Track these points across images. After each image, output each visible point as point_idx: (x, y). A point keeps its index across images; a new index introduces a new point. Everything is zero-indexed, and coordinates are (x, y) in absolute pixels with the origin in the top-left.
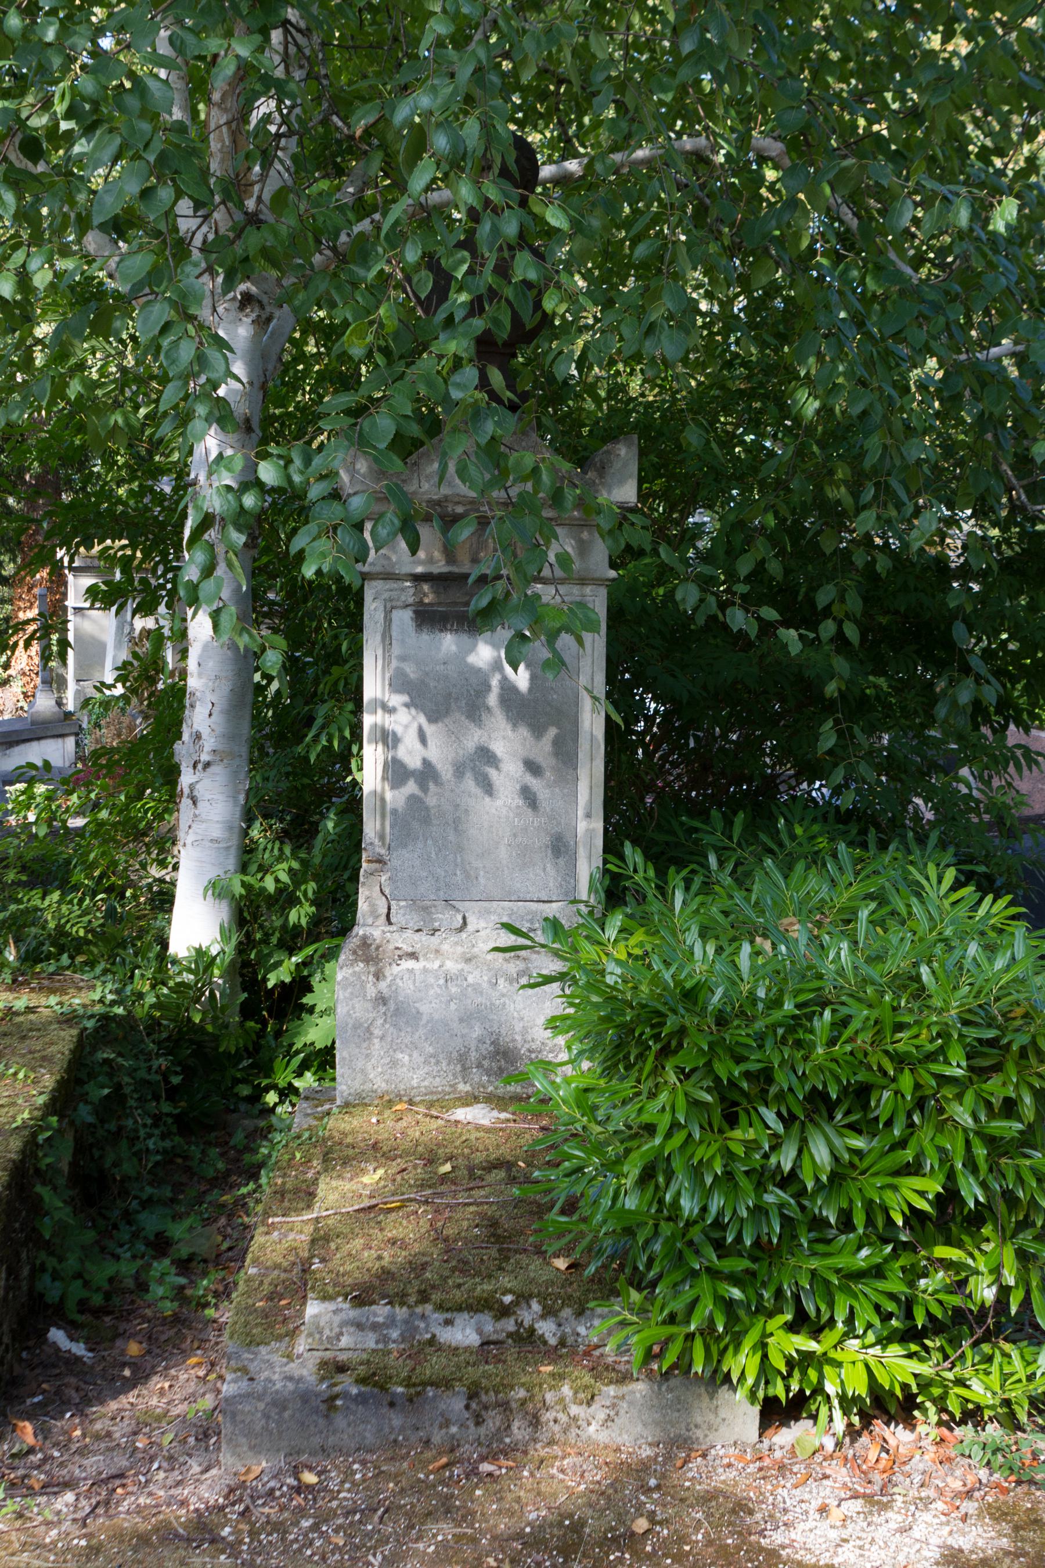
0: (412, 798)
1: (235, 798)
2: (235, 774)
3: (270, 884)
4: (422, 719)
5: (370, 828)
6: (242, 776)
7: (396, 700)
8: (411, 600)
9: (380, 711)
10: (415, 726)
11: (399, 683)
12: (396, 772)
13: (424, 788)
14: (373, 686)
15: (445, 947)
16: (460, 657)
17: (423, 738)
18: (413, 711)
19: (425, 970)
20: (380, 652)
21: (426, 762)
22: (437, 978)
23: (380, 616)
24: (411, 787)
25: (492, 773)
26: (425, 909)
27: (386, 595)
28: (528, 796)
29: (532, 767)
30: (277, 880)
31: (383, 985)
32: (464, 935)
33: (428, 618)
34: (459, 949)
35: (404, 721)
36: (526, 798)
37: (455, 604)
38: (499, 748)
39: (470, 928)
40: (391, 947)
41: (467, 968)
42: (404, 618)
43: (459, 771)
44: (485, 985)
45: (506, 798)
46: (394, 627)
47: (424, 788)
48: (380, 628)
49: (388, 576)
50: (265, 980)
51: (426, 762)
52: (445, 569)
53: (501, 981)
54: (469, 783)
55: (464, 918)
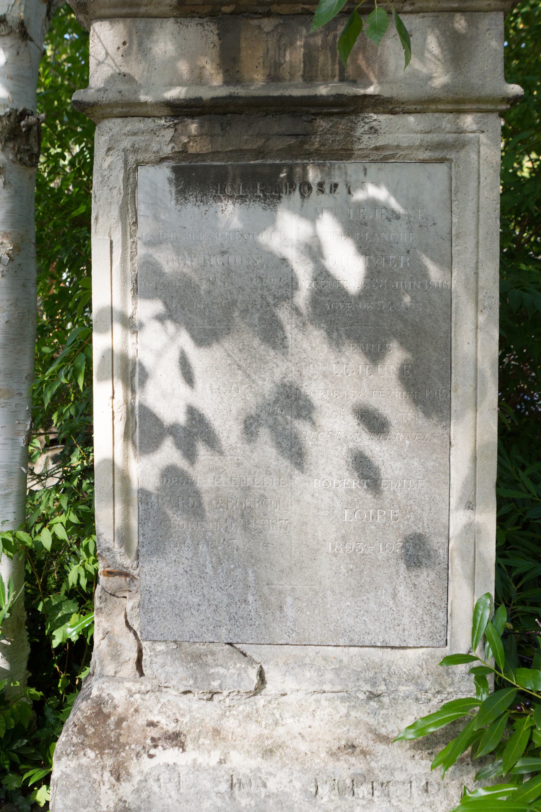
0: (170, 473)
1: (13, 440)
2: (14, 414)
3: (46, 539)
4: (185, 340)
5: (107, 517)
6: (22, 416)
7: (146, 309)
8: (167, 150)
9: (117, 328)
10: (173, 356)
11: (146, 282)
12: (144, 429)
13: (190, 455)
14: (107, 287)
15: (230, 724)
16: (248, 236)
17: (187, 374)
18: (170, 326)
19: (195, 767)
20: (117, 237)
21: (192, 412)
22: (215, 781)
23: (118, 176)
24: (168, 453)
25: (303, 428)
26: (197, 658)
27: (126, 143)
28: (365, 469)
29: (373, 422)
30: (54, 535)
31: (126, 789)
32: (260, 700)
33: (195, 179)
34: (254, 730)
35: (158, 345)
36: (363, 476)
37: (241, 153)
38: (315, 391)
39: (270, 688)
40: (141, 721)
41: (266, 766)
42: (157, 179)
43: (250, 427)
44: (297, 797)
45: (328, 476)
46: (140, 196)
47: (190, 455)
48: (117, 196)
49: (130, 110)
50: (51, 637)
51: (192, 412)
52: (224, 92)
53: (324, 790)
54: (266, 449)
55: (261, 674)
